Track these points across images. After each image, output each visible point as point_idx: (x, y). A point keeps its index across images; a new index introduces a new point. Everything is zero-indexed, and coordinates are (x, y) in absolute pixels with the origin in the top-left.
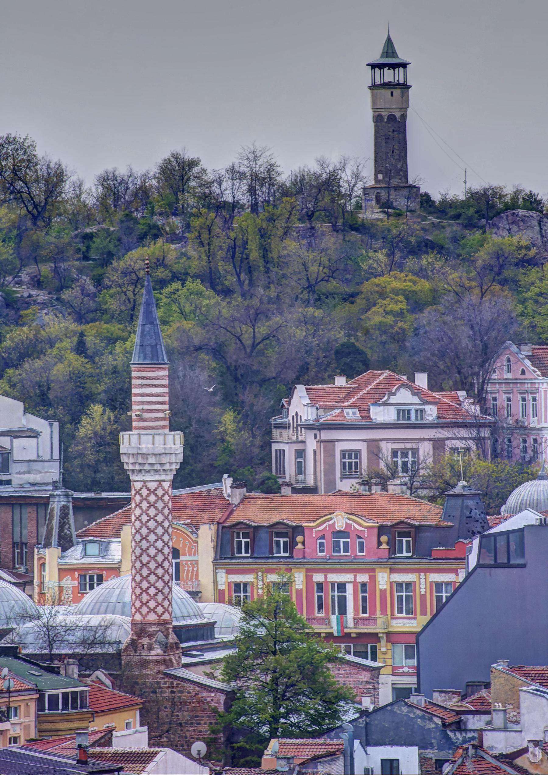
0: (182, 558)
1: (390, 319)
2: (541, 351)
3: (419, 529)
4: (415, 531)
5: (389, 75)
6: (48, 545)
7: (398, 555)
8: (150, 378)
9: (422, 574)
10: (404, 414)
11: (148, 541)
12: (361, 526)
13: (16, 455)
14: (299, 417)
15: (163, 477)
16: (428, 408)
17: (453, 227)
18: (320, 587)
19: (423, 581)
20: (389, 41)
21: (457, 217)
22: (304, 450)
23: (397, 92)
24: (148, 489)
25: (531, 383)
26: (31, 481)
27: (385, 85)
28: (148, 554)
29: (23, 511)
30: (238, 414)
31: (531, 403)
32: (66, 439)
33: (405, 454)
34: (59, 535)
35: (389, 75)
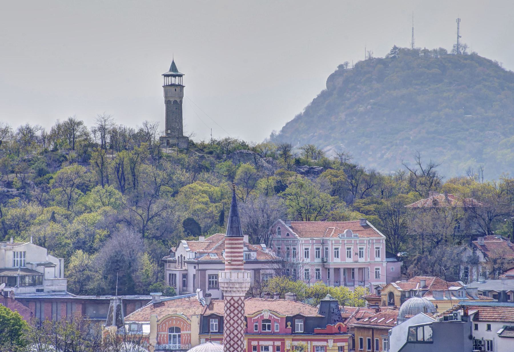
0: (182, 332)
2: (295, 224)
7: (296, 332)
8: (236, 244)
9: (309, 342)
11: (234, 327)
13: (47, 276)
14: (183, 258)
15: (241, 295)
16: (252, 253)
19: (309, 345)
20: (173, 63)
21: (211, 153)
22: (187, 274)
23: (178, 89)
24: (234, 300)
25: (293, 241)
26: (53, 289)
27: (172, 85)
28: (233, 334)
29: (73, 306)
30: (150, 255)
31: (292, 250)
34: (116, 320)
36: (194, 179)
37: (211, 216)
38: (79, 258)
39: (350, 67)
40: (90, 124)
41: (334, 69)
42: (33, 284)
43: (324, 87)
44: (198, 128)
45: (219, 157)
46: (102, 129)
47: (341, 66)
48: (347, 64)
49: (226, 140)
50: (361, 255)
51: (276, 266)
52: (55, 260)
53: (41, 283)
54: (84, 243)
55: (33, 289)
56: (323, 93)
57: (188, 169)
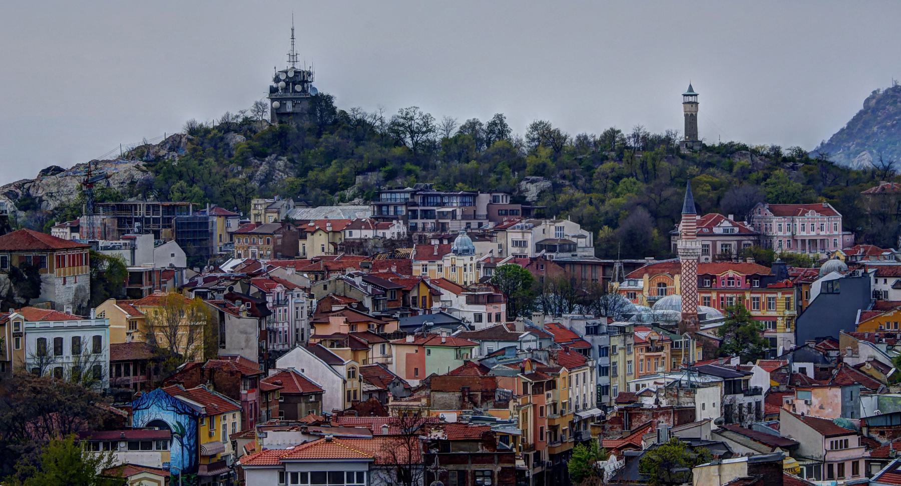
1: (706, 193)
3: (762, 277)
4: (761, 278)
5: (691, 99)
6: (614, 281)
10: (726, 230)
12: (738, 275)
17: (717, 158)
18: (722, 299)
21: (718, 153)
27: (689, 103)
32: (595, 238)
33: (726, 245)
35: (691, 99)
36: (702, 172)
37: (710, 200)
38: (605, 231)
39: (881, 92)
40: (627, 132)
41: (869, 94)
42: (569, 251)
43: (862, 108)
44: (711, 133)
45: (724, 156)
46: (636, 136)
47: (874, 92)
48: (879, 90)
49: (730, 143)
50: (822, 229)
51: (752, 238)
52: (586, 233)
53: (575, 250)
54: (612, 220)
55: (569, 254)
56: (861, 112)
57: (698, 165)
